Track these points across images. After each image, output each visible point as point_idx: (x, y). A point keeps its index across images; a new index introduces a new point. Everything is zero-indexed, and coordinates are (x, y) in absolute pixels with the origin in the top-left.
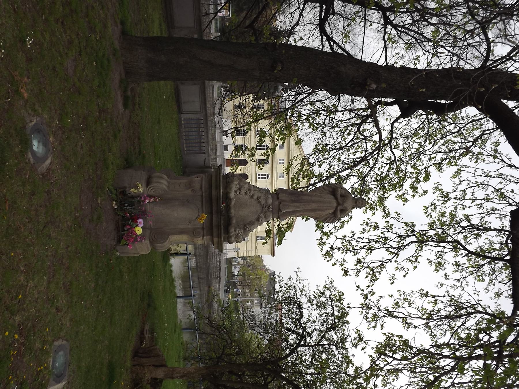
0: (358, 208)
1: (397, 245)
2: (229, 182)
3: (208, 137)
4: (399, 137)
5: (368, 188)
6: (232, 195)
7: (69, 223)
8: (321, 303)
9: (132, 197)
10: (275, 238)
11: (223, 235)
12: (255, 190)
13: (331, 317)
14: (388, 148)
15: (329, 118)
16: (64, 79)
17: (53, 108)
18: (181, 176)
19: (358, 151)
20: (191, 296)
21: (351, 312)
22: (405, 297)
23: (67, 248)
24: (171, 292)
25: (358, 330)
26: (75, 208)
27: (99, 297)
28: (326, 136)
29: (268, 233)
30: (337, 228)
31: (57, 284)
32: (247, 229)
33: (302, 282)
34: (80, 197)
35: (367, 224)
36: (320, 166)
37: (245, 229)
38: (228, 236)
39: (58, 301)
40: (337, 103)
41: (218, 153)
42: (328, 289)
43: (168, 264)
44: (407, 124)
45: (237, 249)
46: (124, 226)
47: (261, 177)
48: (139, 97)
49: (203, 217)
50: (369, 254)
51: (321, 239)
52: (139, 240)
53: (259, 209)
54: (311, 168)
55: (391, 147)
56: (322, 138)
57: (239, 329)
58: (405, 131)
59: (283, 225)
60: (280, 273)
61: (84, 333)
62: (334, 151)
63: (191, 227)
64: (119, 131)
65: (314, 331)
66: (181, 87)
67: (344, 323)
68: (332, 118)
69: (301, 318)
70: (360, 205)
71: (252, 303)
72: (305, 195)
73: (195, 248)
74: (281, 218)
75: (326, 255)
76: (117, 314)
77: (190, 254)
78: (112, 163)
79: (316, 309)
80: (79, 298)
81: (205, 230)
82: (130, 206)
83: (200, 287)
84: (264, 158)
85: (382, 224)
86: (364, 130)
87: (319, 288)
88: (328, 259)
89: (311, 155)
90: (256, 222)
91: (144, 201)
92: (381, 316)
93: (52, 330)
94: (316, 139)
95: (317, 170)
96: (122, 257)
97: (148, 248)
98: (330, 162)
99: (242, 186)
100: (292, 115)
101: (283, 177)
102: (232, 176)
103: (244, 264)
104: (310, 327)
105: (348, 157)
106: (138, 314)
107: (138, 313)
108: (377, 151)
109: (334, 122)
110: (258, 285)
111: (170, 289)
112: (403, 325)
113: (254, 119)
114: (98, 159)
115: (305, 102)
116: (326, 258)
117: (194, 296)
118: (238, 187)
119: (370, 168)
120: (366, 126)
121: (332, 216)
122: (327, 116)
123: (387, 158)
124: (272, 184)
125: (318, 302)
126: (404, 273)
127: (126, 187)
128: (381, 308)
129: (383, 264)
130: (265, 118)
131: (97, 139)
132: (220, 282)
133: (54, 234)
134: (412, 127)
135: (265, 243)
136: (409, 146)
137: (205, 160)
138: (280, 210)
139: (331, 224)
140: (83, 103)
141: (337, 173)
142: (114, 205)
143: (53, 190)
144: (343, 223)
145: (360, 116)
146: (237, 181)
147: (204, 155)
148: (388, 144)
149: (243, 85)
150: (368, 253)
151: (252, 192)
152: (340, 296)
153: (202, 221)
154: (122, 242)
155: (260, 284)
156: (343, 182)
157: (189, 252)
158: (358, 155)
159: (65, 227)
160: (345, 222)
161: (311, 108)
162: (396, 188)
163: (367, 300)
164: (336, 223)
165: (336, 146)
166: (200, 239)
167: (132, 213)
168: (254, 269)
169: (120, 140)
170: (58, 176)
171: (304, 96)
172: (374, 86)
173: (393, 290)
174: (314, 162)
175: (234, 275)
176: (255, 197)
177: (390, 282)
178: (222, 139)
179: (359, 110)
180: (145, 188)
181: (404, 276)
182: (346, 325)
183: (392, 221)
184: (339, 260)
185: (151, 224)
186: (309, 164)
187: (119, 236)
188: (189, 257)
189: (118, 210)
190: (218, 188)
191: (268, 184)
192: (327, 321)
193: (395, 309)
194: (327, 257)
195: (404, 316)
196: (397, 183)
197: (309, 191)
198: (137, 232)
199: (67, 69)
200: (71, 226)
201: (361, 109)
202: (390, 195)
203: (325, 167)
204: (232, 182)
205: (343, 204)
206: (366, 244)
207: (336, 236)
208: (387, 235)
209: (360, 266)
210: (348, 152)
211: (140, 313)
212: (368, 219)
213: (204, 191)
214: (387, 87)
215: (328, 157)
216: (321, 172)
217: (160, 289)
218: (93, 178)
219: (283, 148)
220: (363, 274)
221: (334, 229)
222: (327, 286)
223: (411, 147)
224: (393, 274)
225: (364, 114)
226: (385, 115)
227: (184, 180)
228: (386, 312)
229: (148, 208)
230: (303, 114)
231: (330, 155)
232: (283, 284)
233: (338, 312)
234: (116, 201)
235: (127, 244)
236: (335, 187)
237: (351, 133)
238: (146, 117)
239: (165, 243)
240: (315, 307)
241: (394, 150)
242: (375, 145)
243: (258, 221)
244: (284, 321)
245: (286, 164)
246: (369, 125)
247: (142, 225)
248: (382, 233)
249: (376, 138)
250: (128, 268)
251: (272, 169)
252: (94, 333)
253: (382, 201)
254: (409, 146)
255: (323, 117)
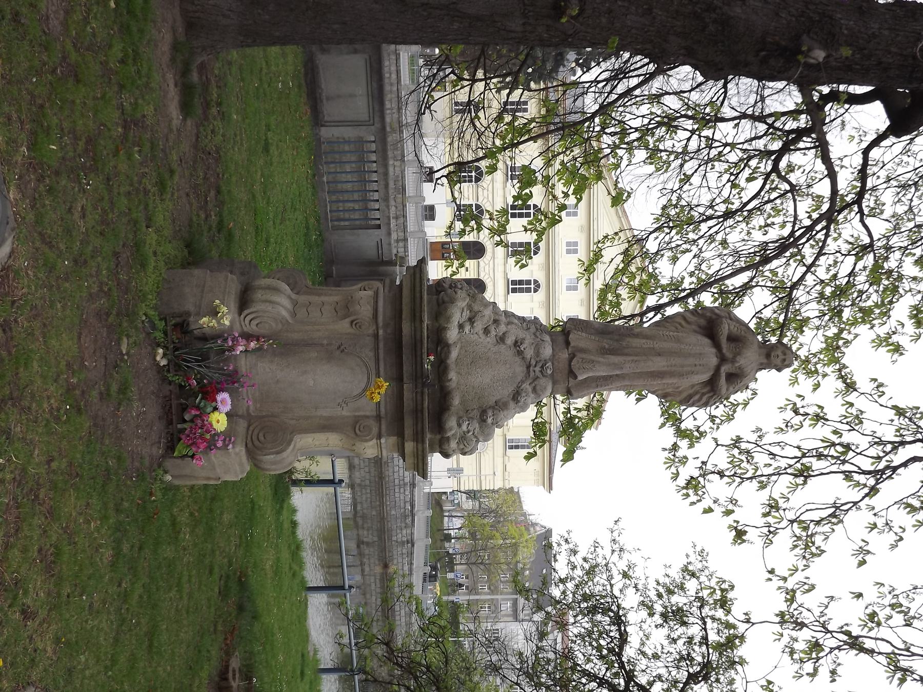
0: (774, 370)
1: (873, 464)
2: (444, 302)
3: (387, 186)
4: (885, 185)
5: (798, 318)
6: (452, 334)
7: (52, 401)
8: (673, 612)
9: (204, 338)
10: (554, 444)
11: (428, 436)
12: (509, 323)
13: (700, 646)
14: (853, 214)
15: (700, 137)
16: (41, 45)
17: (14, 116)
18: (320, 284)
19: (773, 224)
20: (342, 588)
21: (752, 635)
22: (894, 601)
23: (49, 461)
24: (294, 575)
25: (770, 682)
26: (68, 365)
27: (124, 585)
28: (691, 184)
29: (540, 430)
30: (718, 421)
31: (25, 550)
32: (490, 420)
33: (626, 556)
34: (79, 338)
35: (796, 412)
36: (674, 260)
37: (483, 421)
38: (442, 437)
39: (26, 593)
40: (721, 98)
41: (411, 227)
42: (693, 575)
43: (285, 506)
44: (906, 151)
45: (456, 472)
46: (184, 409)
47: (518, 286)
48: (219, 87)
49: (379, 387)
50: (800, 487)
51: (675, 447)
52: (220, 444)
53: (520, 370)
54: (650, 266)
55: (861, 211)
56: (680, 188)
57: (461, 672)
58: (900, 170)
59: (579, 410)
60: (569, 532)
61: (87, 673)
62: (711, 223)
63: (348, 414)
64: (172, 172)
65: (654, 681)
66: (322, 60)
67: (732, 664)
68: (707, 138)
69: (621, 648)
70: (778, 361)
71: (493, 608)
72: (637, 336)
73: (351, 467)
74: (575, 394)
75: (686, 488)
76: (165, 627)
77: (341, 481)
78: (155, 253)
79: (661, 625)
80: (76, 585)
81: (383, 422)
82: (197, 361)
83: (362, 564)
84: (531, 237)
85: (835, 410)
86: (791, 168)
87: (669, 572)
88: (693, 498)
89: (651, 233)
90: (512, 404)
91: (232, 349)
92: (831, 648)
93: (12, 664)
94: (664, 192)
95: (665, 270)
96: (177, 488)
97: (241, 465)
98: (700, 249)
99: (476, 313)
100: (603, 129)
101: (575, 288)
102: (451, 287)
103: (473, 510)
104: (643, 671)
105: (746, 238)
106: (215, 630)
107: (215, 626)
108: (824, 223)
109: (711, 148)
110: (508, 564)
111: (291, 568)
112: (886, 671)
113: (506, 143)
114: (122, 243)
115: (637, 96)
116: (687, 495)
117: (350, 587)
118: (466, 314)
119: (804, 265)
120: (796, 158)
121: (705, 390)
122: (693, 132)
123: (851, 240)
124: (549, 304)
125: (665, 607)
126: (891, 538)
127: (188, 314)
128: (830, 628)
129: (837, 513)
130: (534, 139)
131: (119, 194)
132: (412, 553)
133: (19, 429)
134: (919, 158)
135: (529, 457)
136: (910, 209)
137: (379, 246)
138: (572, 374)
139: (702, 411)
140: (85, 103)
141: (716, 281)
142: (158, 358)
143: (16, 321)
144: (735, 406)
145: (780, 130)
146: (464, 300)
147: (376, 232)
148: (853, 203)
149: (478, 53)
150: (797, 485)
151: (503, 328)
152: (722, 590)
153: (377, 398)
154: (177, 450)
155: (514, 561)
156: (733, 302)
157: (338, 477)
158: (774, 234)
159: (44, 411)
160: (738, 405)
161: (653, 110)
162: (874, 319)
163: (795, 605)
164: (714, 407)
165: (716, 208)
166: (371, 443)
167: (203, 378)
168: (499, 522)
169: (173, 195)
170: (29, 287)
171: (634, 82)
172: (820, 55)
173: (863, 580)
174: (658, 251)
175: (448, 538)
176: (510, 341)
177: (856, 562)
178: (419, 191)
179: (777, 115)
180: (236, 316)
181: (894, 547)
182: (739, 667)
183: (860, 402)
184: (722, 501)
185: (249, 406)
186: (645, 255)
187: (172, 434)
188: (339, 489)
189: (168, 371)
190: (416, 317)
191: (535, 305)
192: (689, 658)
193: (866, 629)
194: (691, 492)
195: (889, 649)
196: (877, 305)
197: (646, 325)
198: (215, 425)
199: (48, 18)
200: (58, 410)
201: (784, 114)
202: (856, 336)
203: (686, 262)
204: (452, 301)
205: (733, 361)
206: (792, 462)
207: (716, 440)
208: (847, 438)
209: (774, 517)
210: (747, 224)
211: (220, 628)
212: (799, 396)
213: (381, 324)
214: (853, 55)
215: (696, 237)
216: (676, 275)
217: (268, 567)
218: (110, 289)
219: (575, 214)
220: (784, 538)
221: (709, 424)
222: (690, 568)
223: (916, 211)
224: (863, 541)
225: (791, 125)
226: (847, 127)
227: (332, 297)
228: (845, 638)
229: (244, 365)
230: (631, 128)
231: (701, 233)
232: (578, 560)
233: (718, 633)
234: (165, 348)
235: (190, 454)
236: (714, 317)
237: (755, 175)
238: (235, 135)
239: (285, 454)
240: (658, 619)
241: (869, 221)
242: (818, 207)
243: (516, 400)
244: (580, 656)
245: (582, 254)
246: (805, 154)
247: (228, 408)
248: (835, 432)
249: (823, 188)
250: (191, 514)
251: (549, 267)
252: (110, 673)
253: (833, 349)
254: (910, 209)
255: (682, 135)
